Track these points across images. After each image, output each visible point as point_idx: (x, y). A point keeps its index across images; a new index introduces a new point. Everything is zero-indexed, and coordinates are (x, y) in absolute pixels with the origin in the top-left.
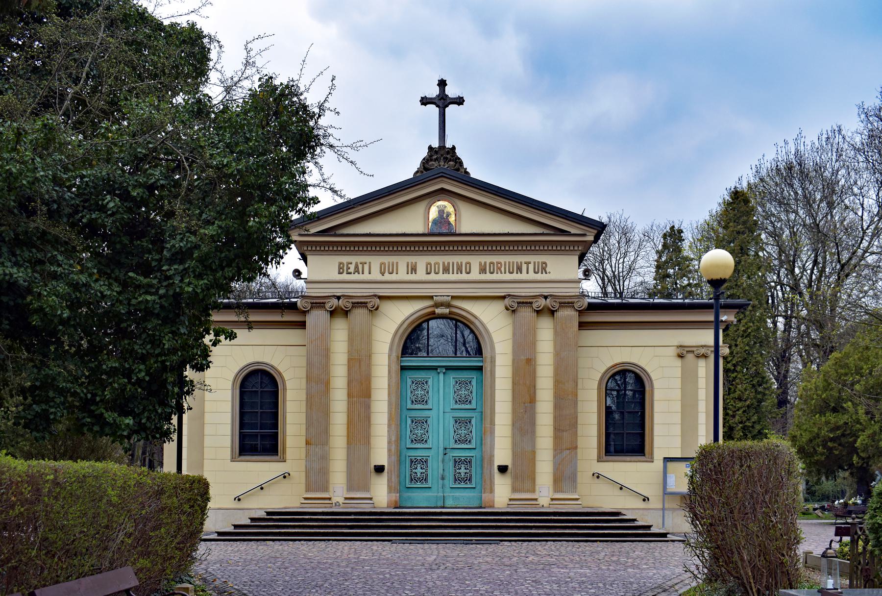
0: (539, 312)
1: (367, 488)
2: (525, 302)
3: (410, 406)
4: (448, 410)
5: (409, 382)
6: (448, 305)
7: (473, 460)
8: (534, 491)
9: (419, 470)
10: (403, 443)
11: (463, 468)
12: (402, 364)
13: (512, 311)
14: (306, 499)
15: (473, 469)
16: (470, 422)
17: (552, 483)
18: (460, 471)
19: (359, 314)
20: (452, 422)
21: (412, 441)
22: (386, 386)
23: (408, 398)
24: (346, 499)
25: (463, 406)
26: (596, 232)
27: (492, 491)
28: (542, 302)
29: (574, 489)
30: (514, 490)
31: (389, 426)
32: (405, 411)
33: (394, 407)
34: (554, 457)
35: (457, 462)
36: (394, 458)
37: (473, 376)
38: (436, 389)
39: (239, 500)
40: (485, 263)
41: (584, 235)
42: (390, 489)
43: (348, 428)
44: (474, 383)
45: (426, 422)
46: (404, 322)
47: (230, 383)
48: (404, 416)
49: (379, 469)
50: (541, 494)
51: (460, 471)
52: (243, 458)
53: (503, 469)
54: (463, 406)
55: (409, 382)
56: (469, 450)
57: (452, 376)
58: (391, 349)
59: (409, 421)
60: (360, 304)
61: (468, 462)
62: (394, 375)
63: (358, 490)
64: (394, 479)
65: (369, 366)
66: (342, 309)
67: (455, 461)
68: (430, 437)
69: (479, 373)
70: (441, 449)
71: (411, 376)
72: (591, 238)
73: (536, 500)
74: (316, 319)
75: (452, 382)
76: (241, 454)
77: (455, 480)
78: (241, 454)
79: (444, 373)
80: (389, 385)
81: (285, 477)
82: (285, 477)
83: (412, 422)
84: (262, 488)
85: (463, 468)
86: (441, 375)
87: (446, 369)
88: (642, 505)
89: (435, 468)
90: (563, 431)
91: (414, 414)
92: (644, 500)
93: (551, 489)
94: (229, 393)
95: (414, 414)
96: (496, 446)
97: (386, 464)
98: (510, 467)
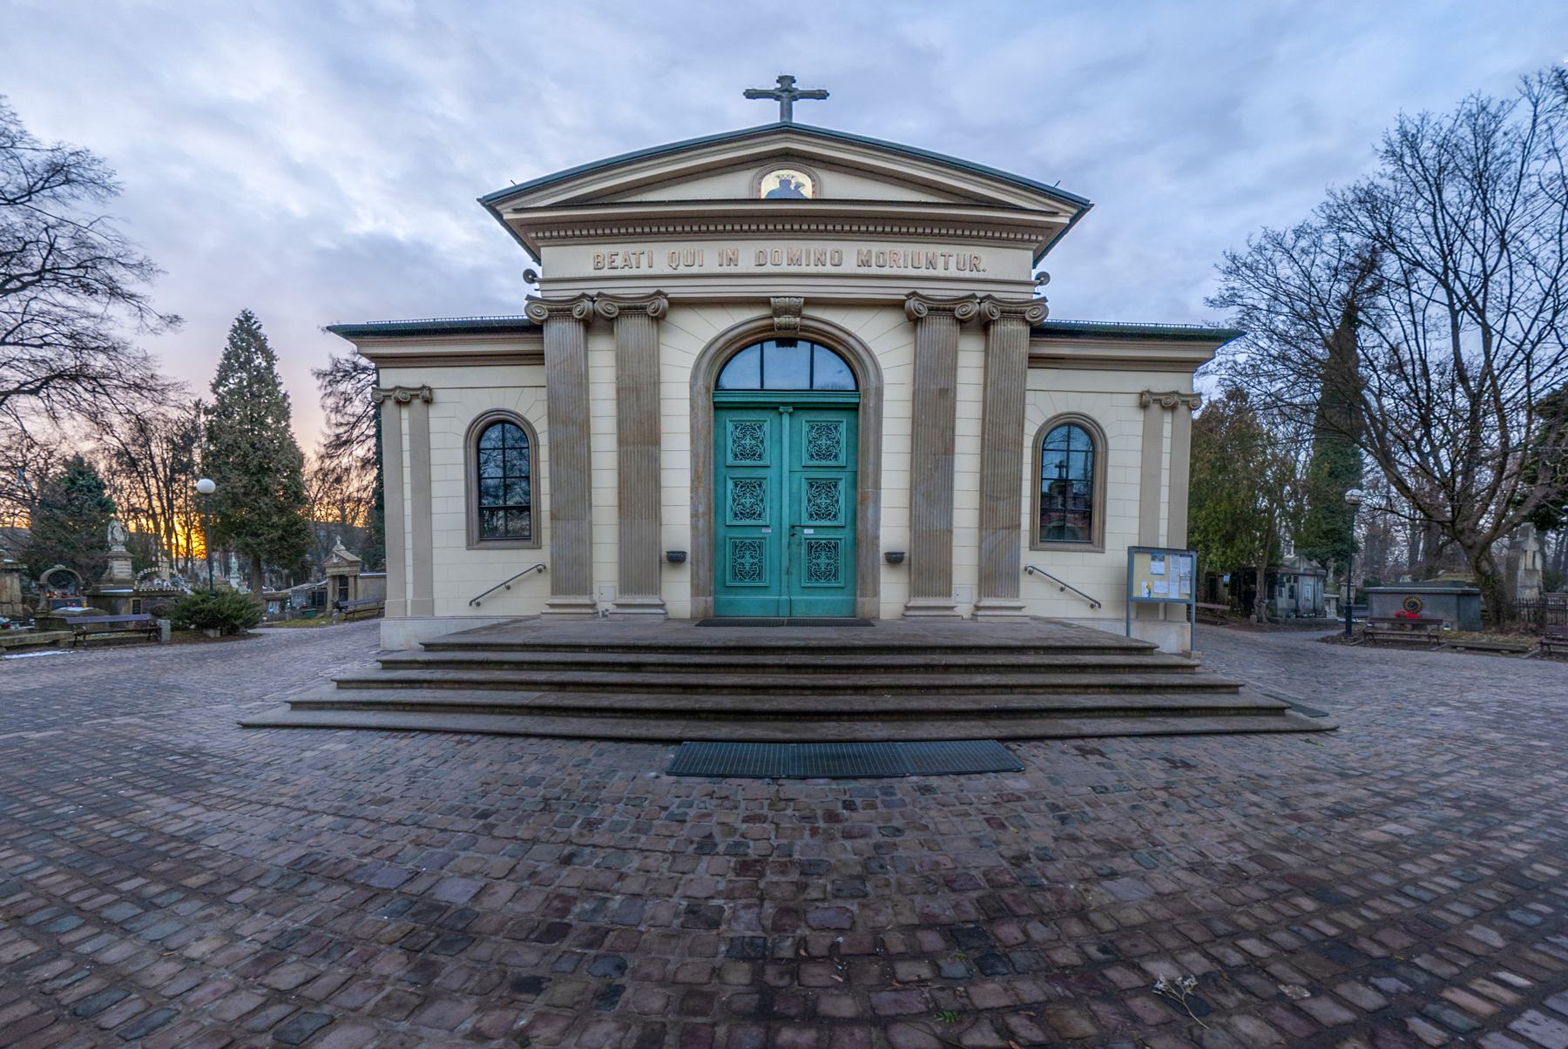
0: (962, 323)
1: (655, 588)
2: (941, 309)
3: (730, 460)
4: (797, 467)
5: (730, 427)
6: (797, 312)
7: (841, 545)
8: (950, 595)
9: (823, 560)
10: (720, 520)
11: (823, 557)
12: (716, 400)
13: (915, 321)
14: (552, 606)
15: (841, 559)
16: (835, 486)
17: (976, 582)
18: (819, 561)
19: (633, 329)
20: (805, 486)
21: (736, 515)
22: (688, 429)
23: (729, 451)
24: (618, 606)
25: (824, 463)
26: (1075, 211)
27: (876, 593)
28: (973, 308)
29: (1016, 592)
30: (915, 591)
31: (694, 489)
32: (723, 470)
33: (701, 459)
34: (981, 541)
35: (813, 547)
36: (704, 540)
37: (844, 420)
38: (776, 437)
39: (478, 604)
40: (869, 252)
41: (1054, 214)
42: (696, 590)
43: (620, 493)
44: (843, 428)
45: (760, 486)
46: (717, 339)
47: (462, 439)
48: (721, 478)
49: (676, 559)
50: (958, 599)
51: (819, 561)
52: (483, 544)
53: (894, 559)
54: (824, 463)
55: (730, 427)
56: (832, 530)
57: (804, 419)
58: (694, 376)
59: (730, 485)
60: (633, 309)
61: (831, 547)
62: (701, 414)
63: (640, 590)
64: (704, 574)
65: (656, 399)
66: (601, 315)
67: (810, 547)
68: (768, 509)
69: (852, 414)
70: (786, 525)
71: (730, 419)
72: (1067, 221)
73: (951, 608)
74: (560, 335)
75: (806, 427)
76: (481, 539)
77: (810, 575)
78: (481, 539)
79: (790, 414)
80: (692, 427)
81: (540, 571)
82: (540, 571)
83: (736, 485)
84: (508, 588)
85: (823, 557)
86: (786, 419)
87: (795, 409)
88: (1087, 613)
89: (776, 554)
90: (998, 499)
91: (738, 473)
92: (1092, 606)
93: (975, 592)
94: (461, 452)
95: (738, 473)
96: (883, 522)
97: (687, 548)
98: (907, 555)
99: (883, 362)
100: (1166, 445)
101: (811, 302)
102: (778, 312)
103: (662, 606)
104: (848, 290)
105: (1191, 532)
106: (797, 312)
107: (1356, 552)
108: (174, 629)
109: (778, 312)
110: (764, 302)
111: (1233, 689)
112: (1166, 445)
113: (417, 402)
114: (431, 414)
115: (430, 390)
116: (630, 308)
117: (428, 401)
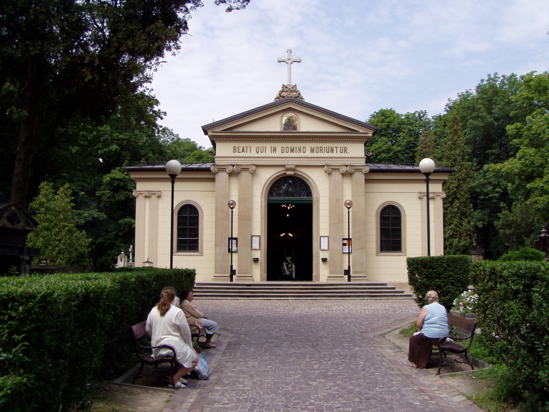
98: (328, 259)
99: (319, 187)
100: (147, 243)
101: (297, 166)
102: (288, 170)
103: (251, 277)
104: (308, 162)
105: (445, 248)
106: (293, 170)
107: (35, 214)
108: (493, 124)
109: (288, 170)
110: (284, 166)
111: (403, 292)
112: (147, 243)
113: (154, 197)
114: (160, 204)
115: (160, 191)
116: (244, 168)
117: (159, 197)
